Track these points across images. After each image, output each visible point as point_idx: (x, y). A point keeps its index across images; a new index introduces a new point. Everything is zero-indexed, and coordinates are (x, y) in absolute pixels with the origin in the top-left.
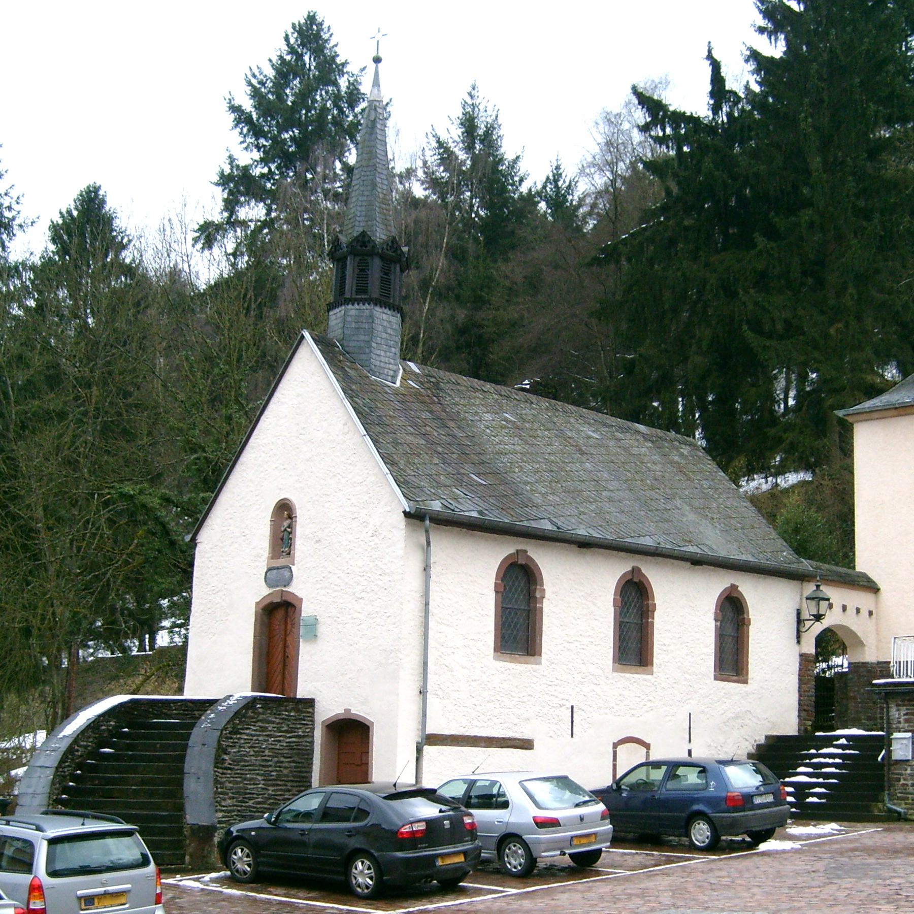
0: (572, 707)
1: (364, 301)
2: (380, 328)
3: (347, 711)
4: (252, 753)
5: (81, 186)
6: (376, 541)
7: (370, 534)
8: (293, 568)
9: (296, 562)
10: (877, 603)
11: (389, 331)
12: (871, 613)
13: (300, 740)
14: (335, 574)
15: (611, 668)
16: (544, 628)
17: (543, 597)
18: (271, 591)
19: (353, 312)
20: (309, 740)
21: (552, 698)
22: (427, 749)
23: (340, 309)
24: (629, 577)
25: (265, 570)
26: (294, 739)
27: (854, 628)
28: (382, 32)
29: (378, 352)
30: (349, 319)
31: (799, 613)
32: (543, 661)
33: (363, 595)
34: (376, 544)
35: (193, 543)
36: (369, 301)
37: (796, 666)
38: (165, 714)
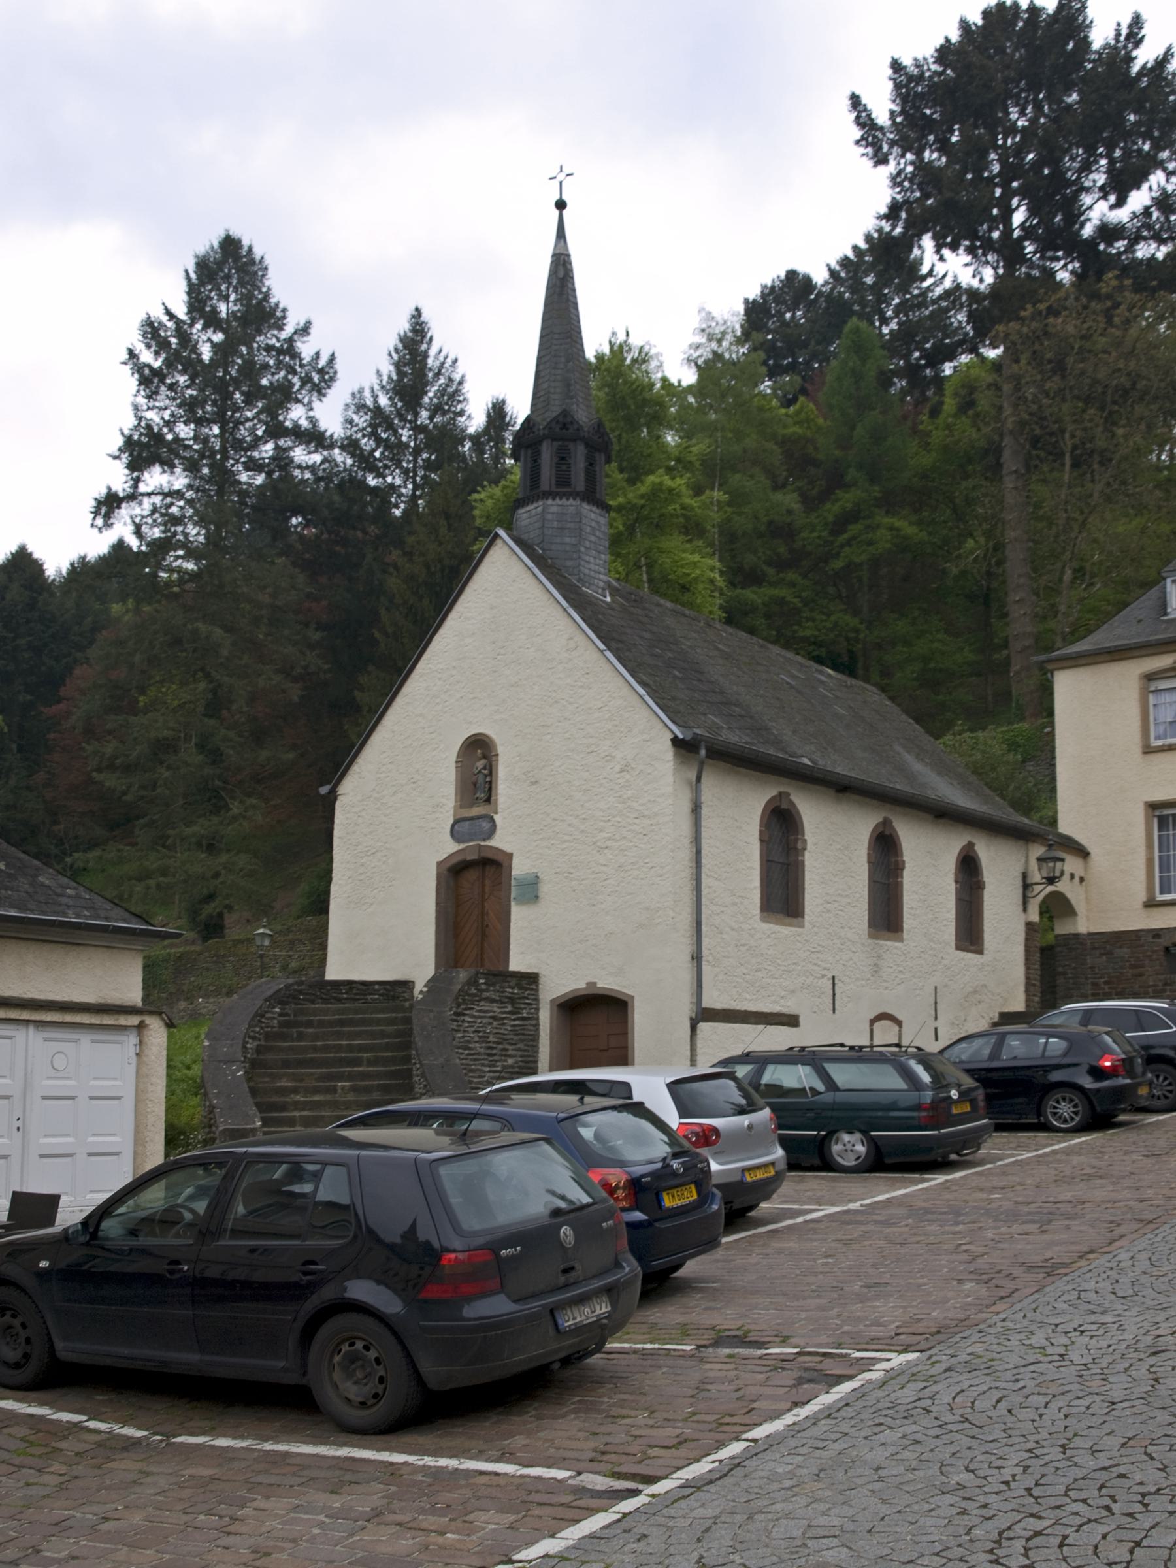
0: (833, 978)
1: (567, 495)
2: (588, 529)
3: (592, 985)
4: (477, 1039)
5: (958, 19)
6: (628, 777)
7: (618, 768)
8: (496, 817)
9: (499, 810)
10: (1086, 869)
11: (598, 533)
12: (1082, 880)
13: (526, 1023)
14: (563, 821)
15: (866, 932)
16: (807, 885)
17: (805, 849)
18: (462, 846)
19: (554, 509)
20: (534, 1022)
21: (816, 968)
22: (704, 1027)
23: (535, 505)
24: (881, 830)
25: (451, 821)
26: (517, 1022)
27: (1069, 895)
28: (566, 171)
29: (587, 558)
30: (549, 517)
31: (1025, 876)
32: (806, 924)
33: (609, 843)
34: (627, 781)
35: (332, 797)
36: (574, 495)
37: (1021, 937)
38: (335, 998)
